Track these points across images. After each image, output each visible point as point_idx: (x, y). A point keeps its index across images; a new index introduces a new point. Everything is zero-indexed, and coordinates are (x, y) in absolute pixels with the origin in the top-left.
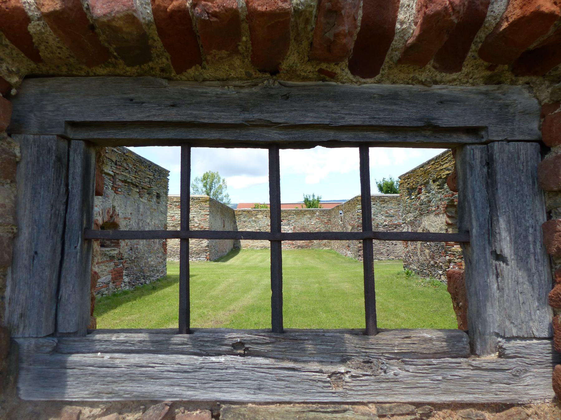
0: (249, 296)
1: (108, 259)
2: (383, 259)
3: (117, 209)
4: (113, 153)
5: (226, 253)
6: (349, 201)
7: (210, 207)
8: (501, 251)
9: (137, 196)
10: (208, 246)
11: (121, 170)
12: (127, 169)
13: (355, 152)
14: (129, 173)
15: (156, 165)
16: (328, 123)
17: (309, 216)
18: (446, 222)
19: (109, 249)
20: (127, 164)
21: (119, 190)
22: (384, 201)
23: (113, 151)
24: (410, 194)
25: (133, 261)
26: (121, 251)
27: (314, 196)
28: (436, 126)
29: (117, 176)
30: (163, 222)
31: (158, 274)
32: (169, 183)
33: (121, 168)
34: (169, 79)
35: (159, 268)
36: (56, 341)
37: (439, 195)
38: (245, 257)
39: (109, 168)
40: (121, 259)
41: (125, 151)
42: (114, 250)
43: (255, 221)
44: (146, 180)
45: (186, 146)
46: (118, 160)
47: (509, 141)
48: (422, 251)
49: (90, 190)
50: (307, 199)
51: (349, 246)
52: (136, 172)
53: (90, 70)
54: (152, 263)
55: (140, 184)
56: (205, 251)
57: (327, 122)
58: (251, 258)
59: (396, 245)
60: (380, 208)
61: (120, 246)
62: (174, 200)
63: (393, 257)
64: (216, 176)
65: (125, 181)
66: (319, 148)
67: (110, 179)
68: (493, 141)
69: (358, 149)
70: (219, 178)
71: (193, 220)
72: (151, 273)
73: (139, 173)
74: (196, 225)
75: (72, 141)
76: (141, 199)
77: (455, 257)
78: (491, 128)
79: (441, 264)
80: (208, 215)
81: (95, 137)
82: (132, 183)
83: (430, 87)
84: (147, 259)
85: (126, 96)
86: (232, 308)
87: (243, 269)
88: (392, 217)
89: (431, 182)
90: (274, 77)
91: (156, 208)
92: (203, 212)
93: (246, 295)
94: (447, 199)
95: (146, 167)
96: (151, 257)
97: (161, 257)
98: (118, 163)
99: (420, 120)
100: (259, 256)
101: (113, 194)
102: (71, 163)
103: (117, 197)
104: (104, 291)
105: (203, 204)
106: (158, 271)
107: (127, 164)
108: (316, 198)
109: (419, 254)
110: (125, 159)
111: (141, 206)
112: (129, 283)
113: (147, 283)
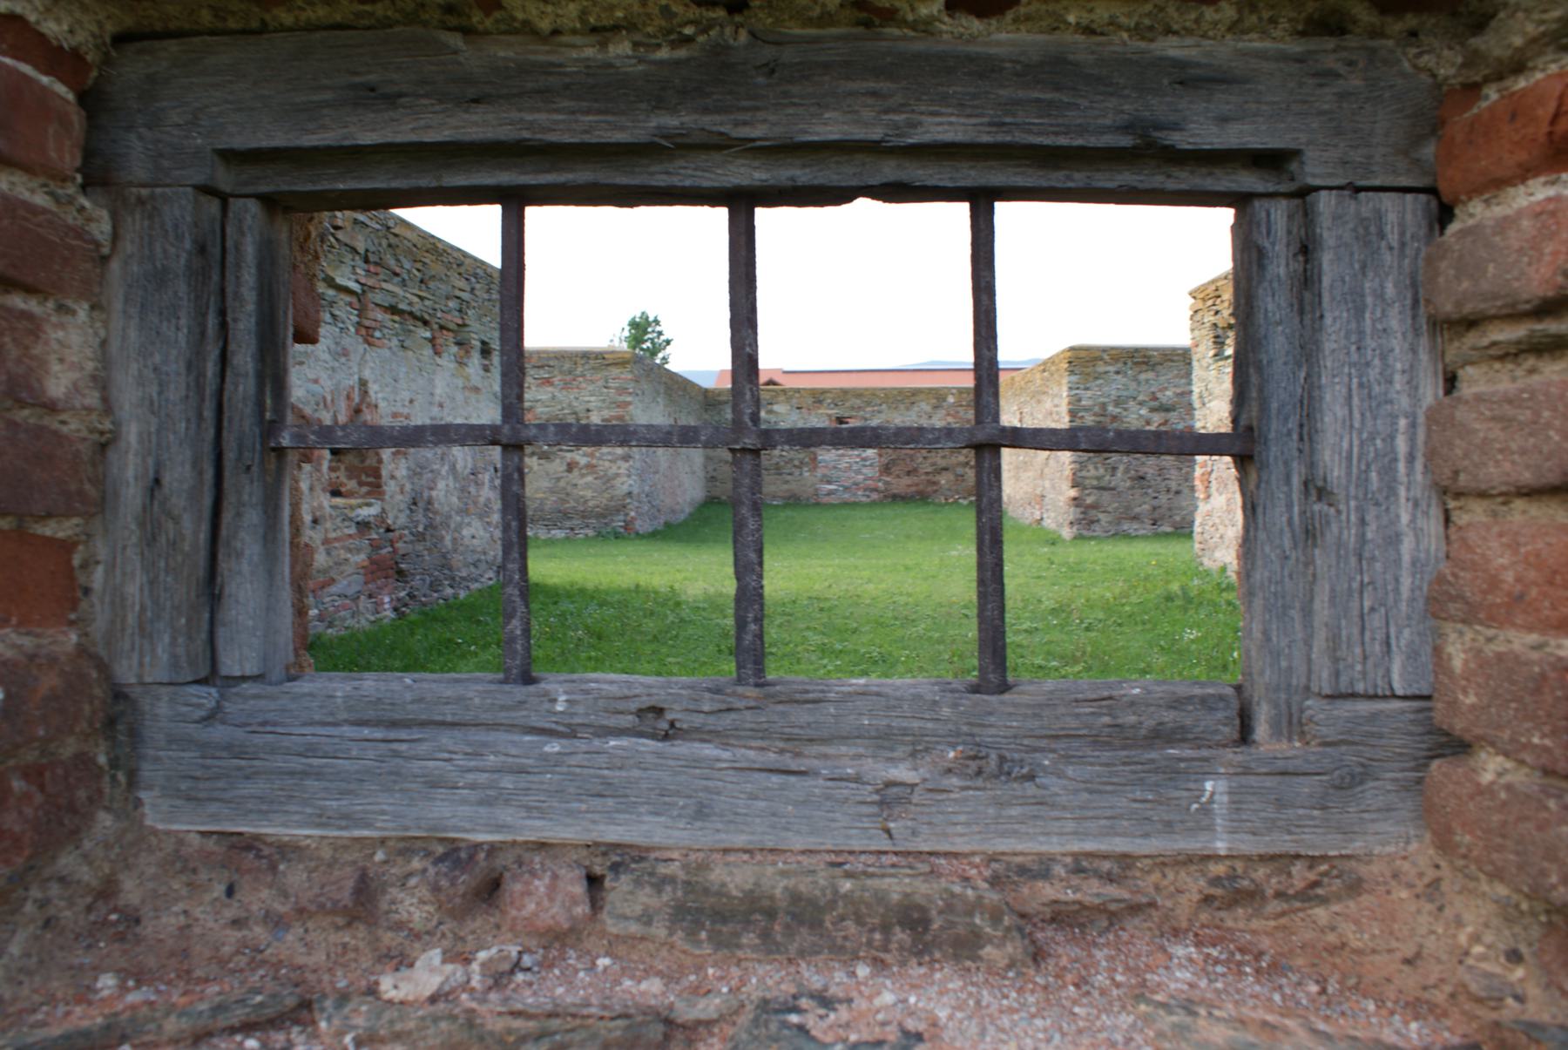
1: (353, 531)
3: (373, 388)
4: (357, 228)
6: (1045, 363)
8: (1325, 480)
9: (428, 351)
11: (381, 277)
12: (397, 275)
13: (958, 213)
14: (404, 284)
15: (476, 259)
16: (876, 137)
19: (353, 502)
20: (398, 260)
21: (377, 334)
23: (356, 221)
25: (420, 537)
28: (1166, 147)
29: (370, 295)
33: (379, 270)
34: (468, 32)
36: (216, 695)
39: (347, 270)
41: (391, 223)
42: (369, 505)
44: (451, 304)
45: (514, 203)
46: (372, 249)
47: (1358, 190)
49: (284, 327)
52: (422, 281)
53: (268, 17)
55: (434, 316)
57: (876, 134)
61: (383, 493)
65: (393, 310)
66: (863, 204)
67: (350, 304)
68: (1318, 189)
69: (966, 206)
72: (472, 569)
73: (432, 285)
75: (231, 200)
76: (439, 361)
78: (1310, 154)
81: (285, 188)
82: (411, 313)
83: (1152, 40)
85: (357, 79)
88: (1167, 410)
90: (738, 18)
95: (449, 266)
96: (469, 524)
98: (372, 258)
99: (1127, 128)
101: (362, 347)
102: (230, 258)
103: (373, 355)
104: (344, 619)
107: (398, 260)
110: (390, 246)
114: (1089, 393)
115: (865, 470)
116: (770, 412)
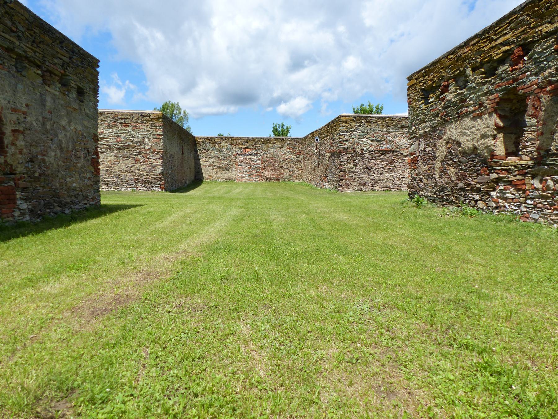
0: (211, 230)
2: (367, 189)
5: (186, 185)
7: (164, 126)
9: (39, 81)
10: (162, 173)
14: (19, 38)
17: (279, 145)
18: (496, 125)
22: (370, 122)
24: (426, 99)
26: (9, 160)
27: (283, 126)
30: (92, 131)
31: (86, 202)
32: (99, 77)
35: (86, 193)
37: (485, 87)
38: (207, 188)
40: (11, 174)
43: (218, 150)
48: (443, 171)
50: (277, 129)
51: (326, 177)
54: (74, 185)
56: (159, 179)
58: (215, 189)
59: (381, 174)
60: (365, 131)
61: (6, 152)
62: (119, 117)
63: (378, 188)
64: (176, 106)
70: (180, 109)
71: (143, 142)
72: (73, 198)
73: (42, 46)
74: (147, 148)
77: (510, 174)
79: (478, 186)
80: (161, 135)
84: (64, 178)
86: (181, 247)
87: (204, 199)
88: (378, 141)
89: (469, 71)
91: (77, 107)
92: (155, 132)
93: (206, 228)
94: (502, 90)
96: (71, 176)
97: (89, 179)
100: (224, 187)
105: (155, 121)
106: (86, 197)
108: (285, 128)
109: (437, 176)
111: (49, 99)
112: (31, 211)
113: (67, 212)
116: (221, 146)
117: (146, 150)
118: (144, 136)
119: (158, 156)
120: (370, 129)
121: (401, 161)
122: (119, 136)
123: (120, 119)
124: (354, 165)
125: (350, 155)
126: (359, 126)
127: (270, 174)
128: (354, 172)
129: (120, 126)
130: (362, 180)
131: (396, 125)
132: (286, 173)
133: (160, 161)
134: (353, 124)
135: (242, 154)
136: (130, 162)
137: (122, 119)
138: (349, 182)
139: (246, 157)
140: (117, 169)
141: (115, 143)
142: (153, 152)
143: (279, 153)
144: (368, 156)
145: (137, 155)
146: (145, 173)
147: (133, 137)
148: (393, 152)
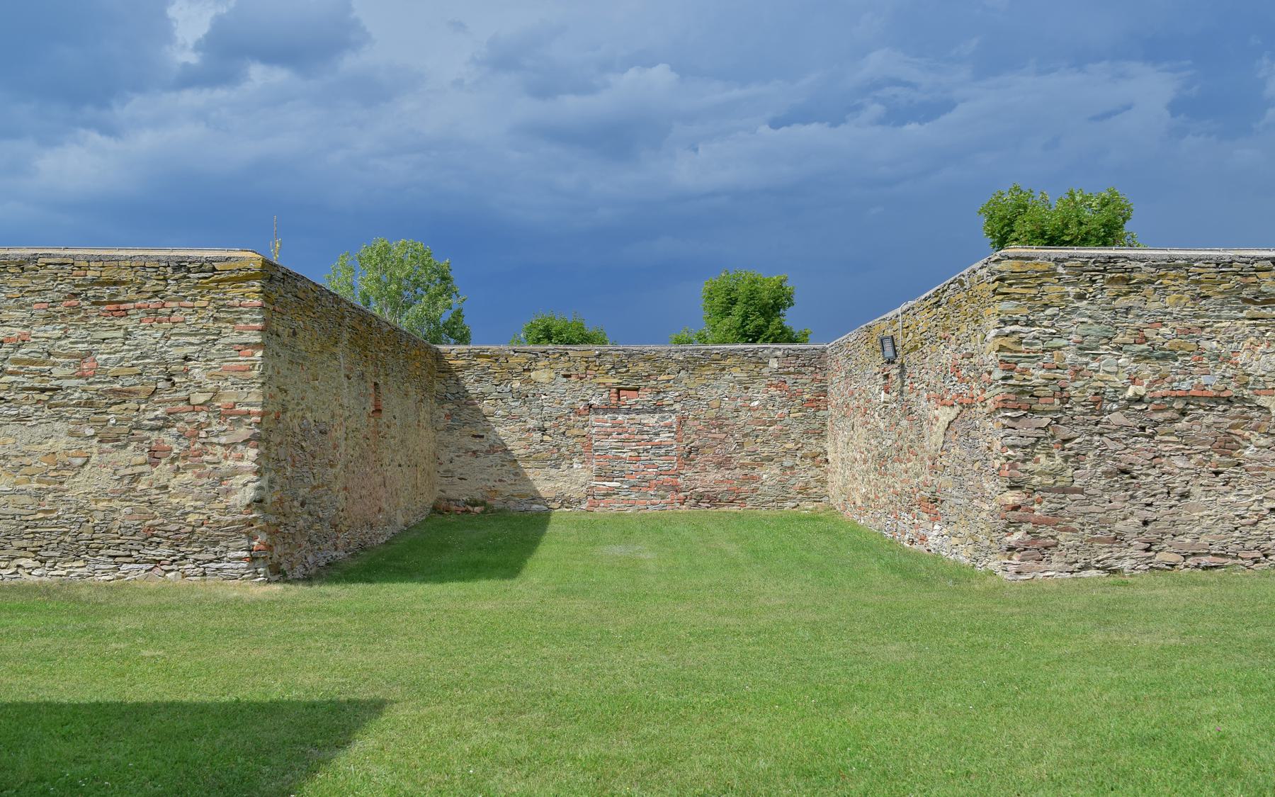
17: (738, 373)
22: (1127, 281)
43: (522, 397)
59: (1184, 496)
60: (1107, 315)
63: (1173, 558)
71: (186, 372)
74: (199, 398)
80: (256, 346)
88: (1164, 357)
114: (1035, 331)
115: (658, 462)
116: (528, 381)
117: (195, 409)
118: (188, 350)
119: (243, 432)
120: (1128, 310)
121: (1263, 442)
122: (90, 353)
123: (94, 282)
124: (1066, 459)
125: (1046, 420)
126: (1081, 297)
127: (711, 478)
128: (1064, 490)
129: (93, 310)
130: (1103, 524)
131: (1235, 292)
132: (769, 474)
133: (252, 453)
134: (1052, 290)
135: (607, 409)
136: (131, 456)
137: (102, 284)
138: (1045, 531)
139: (620, 418)
140: (80, 487)
141: (73, 382)
142: (222, 416)
143: (739, 402)
144: (1123, 421)
145: (160, 429)
146: (189, 503)
147: (144, 356)
148: (1229, 401)
